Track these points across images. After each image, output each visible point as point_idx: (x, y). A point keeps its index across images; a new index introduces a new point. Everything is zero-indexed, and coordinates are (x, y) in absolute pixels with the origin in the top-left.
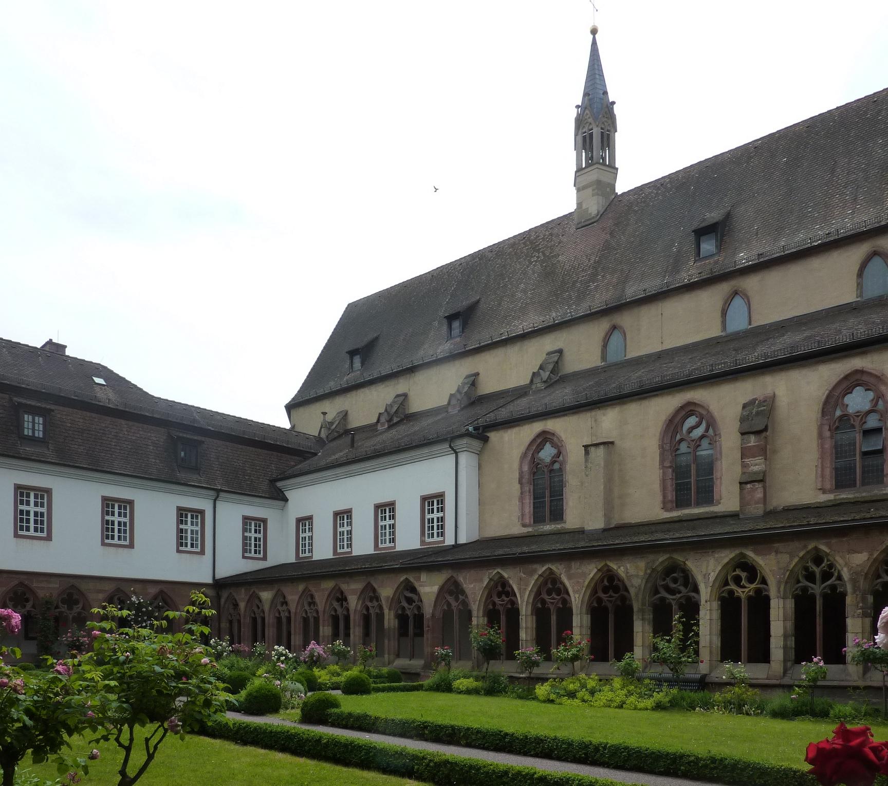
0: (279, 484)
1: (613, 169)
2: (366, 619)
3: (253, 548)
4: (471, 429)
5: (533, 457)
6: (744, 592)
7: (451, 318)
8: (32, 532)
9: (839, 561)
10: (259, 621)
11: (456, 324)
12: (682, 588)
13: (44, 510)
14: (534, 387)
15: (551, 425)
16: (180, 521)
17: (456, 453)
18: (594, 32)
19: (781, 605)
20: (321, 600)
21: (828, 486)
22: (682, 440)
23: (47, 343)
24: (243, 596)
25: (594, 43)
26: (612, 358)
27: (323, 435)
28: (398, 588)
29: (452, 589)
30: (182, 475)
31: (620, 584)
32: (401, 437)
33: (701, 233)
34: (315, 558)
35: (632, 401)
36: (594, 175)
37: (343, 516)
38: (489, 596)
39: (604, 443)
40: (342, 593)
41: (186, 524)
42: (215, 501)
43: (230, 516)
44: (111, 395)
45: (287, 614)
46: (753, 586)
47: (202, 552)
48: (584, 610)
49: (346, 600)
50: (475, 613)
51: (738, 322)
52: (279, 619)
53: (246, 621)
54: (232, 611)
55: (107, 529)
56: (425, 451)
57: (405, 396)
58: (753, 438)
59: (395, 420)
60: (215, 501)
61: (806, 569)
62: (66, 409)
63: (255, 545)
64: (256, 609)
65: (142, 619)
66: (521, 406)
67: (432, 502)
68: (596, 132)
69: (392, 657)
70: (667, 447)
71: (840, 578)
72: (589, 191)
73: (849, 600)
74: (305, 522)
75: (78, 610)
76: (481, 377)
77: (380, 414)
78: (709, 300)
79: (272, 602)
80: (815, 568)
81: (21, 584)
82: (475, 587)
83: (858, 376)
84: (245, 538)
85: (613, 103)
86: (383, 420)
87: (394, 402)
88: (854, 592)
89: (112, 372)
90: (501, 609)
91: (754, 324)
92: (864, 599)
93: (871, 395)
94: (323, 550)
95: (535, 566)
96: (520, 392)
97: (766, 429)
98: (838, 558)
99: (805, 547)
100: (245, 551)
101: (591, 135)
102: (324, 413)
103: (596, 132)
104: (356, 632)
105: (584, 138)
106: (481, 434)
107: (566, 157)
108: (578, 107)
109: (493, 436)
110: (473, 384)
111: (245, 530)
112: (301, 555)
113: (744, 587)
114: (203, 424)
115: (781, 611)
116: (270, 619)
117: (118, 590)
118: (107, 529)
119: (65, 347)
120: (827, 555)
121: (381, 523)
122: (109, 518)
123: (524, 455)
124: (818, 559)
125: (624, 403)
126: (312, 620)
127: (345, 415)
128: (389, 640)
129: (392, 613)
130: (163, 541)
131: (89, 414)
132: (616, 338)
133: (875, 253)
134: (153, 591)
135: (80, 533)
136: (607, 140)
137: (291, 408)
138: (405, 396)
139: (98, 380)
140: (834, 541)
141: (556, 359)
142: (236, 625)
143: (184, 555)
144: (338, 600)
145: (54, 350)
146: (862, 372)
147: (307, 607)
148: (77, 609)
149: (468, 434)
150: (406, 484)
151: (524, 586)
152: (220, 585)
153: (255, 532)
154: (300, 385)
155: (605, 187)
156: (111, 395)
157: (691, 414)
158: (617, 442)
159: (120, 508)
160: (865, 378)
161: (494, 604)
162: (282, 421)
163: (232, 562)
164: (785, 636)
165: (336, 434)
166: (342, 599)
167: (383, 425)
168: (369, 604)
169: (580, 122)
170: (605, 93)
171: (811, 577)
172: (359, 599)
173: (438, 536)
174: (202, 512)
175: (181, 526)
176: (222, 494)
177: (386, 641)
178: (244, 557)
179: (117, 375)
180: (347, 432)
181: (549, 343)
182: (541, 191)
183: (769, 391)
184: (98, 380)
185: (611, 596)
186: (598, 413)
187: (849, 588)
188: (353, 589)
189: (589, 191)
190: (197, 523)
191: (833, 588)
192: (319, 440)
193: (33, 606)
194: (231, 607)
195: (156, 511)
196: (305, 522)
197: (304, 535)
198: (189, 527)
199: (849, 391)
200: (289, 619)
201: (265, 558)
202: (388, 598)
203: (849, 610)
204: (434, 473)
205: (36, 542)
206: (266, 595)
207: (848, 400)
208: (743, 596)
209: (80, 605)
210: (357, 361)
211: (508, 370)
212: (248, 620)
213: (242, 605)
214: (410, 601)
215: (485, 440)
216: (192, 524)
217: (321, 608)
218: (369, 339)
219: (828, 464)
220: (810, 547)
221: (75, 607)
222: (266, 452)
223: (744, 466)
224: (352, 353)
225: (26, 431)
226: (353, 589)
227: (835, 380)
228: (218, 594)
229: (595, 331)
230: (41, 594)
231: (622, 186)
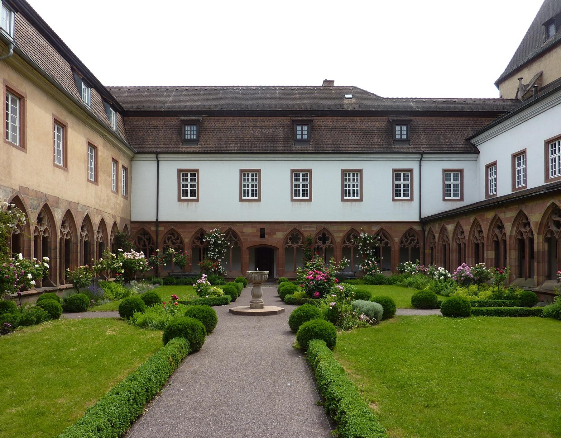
0: (473, 141)
2: (521, 242)
8: (301, 197)
13: (182, 183)
20: (467, 228)
23: (324, 81)
24: (437, 229)
27: (520, 97)
28: (545, 213)
37: (519, 156)
42: (420, 161)
43: (431, 175)
47: (412, 200)
55: (346, 191)
60: (420, 161)
65: (367, 248)
69: (541, 278)
74: (491, 166)
75: (329, 244)
81: (295, 229)
89: (359, 89)
94: (504, 189)
117: (353, 229)
118: (195, 191)
119: (333, 81)
122: (398, 183)
128: (538, 262)
129: (541, 237)
130: (376, 193)
131: (336, 118)
134: (375, 229)
137: (498, 84)
148: (328, 243)
152: (424, 222)
153: (452, 181)
154: (508, 64)
159: (354, 175)
162: (494, 93)
163: (434, 203)
168: (523, 230)
172: (513, 226)
173: (191, 196)
174: (411, 171)
176: (425, 156)
177: (535, 264)
190: (357, 179)
193: (303, 243)
195: (377, 174)
196: (491, 166)
201: (462, 199)
202: (537, 223)
205: (354, 203)
206: (450, 227)
209: (330, 241)
210: (552, 29)
212: (441, 247)
213: (437, 236)
222: (464, 118)
225: (298, 136)
228: (423, 228)
230: (306, 235)
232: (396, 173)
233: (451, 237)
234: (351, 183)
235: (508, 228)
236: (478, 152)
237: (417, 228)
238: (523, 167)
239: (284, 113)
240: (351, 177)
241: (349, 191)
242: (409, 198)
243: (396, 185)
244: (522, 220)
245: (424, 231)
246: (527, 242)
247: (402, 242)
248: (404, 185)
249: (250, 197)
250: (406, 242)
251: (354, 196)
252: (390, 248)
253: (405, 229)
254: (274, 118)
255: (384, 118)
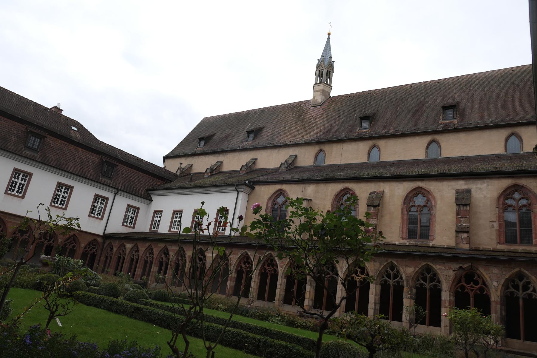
0: (150, 192)
1: (330, 86)
2: (177, 267)
3: (129, 221)
4: (247, 182)
5: (274, 201)
6: (358, 278)
7: (249, 132)
9: (401, 270)
10: (122, 259)
11: (251, 136)
12: (330, 272)
14: (281, 169)
15: (284, 187)
16: (95, 201)
17: (238, 192)
18: (329, 34)
19: (374, 288)
20: (156, 251)
21: (404, 236)
22: (342, 204)
25: (329, 38)
26: (318, 164)
27: (178, 173)
29: (246, 260)
30: (103, 179)
31: (275, 263)
32: (216, 180)
33: (363, 118)
34: (159, 232)
35: (322, 183)
36: (321, 87)
38: (240, 263)
39: (307, 199)
40: (167, 250)
41: (97, 203)
43: (120, 205)
44: (78, 136)
45: (137, 257)
46: (363, 276)
47: (102, 219)
48: (284, 276)
49: (169, 254)
50: (280, 276)
51: (374, 159)
52: (132, 260)
53: (115, 258)
54: (109, 252)
55: (11, 187)
56: (224, 188)
57: (222, 162)
58: (372, 208)
59: (214, 173)
61: (387, 271)
62: (53, 138)
63: (130, 220)
64: (122, 253)
66: (274, 177)
67: (223, 212)
68: (325, 71)
70: (335, 206)
71: (401, 278)
72: (319, 93)
73: (405, 289)
76: (258, 161)
77: (243, 166)
78: (363, 147)
79: (131, 250)
80: (427, 275)
82: (234, 258)
83: (420, 190)
84: (126, 215)
85: (333, 62)
86: (208, 171)
87: (215, 164)
88: (407, 286)
89: (82, 126)
90: (244, 270)
91: (381, 160)
92: (411, 290)
93: (425, 199)
94: (164, 228)
95: (264, 251)
96: (274, 171)
97: (378, 205)
98: (401, 269)
99: (387, 261)
100: (124, 222)
101: (323, 72)
102: (181, 164)
103: (325, 71)
104: (170, 272)
105: (320, 72)
106: (251, 186)
107: (311, 78)
108: (319, 60)
109: (257, 188)
110: (254, 163)
111: (127, 211)
112: (152, 229)
113: (359, 276)
114: (120, 157)
115: (374, 290)
116: (128, 259)
120: (396, 266)
121: (174, 219)
122: (15, 180)
123: (270, 199)
124: (392, 267)
125: (318, 183)
126: (149, 262)
127: (191, 166)
131: (64, 142)
132: (321, 154)
133: (513, 134)
135: (38, 198)
136: (329, 75)
137: (165, 158)
138: (222, 162)
139: (73, 128)
140: (399, 260)
141: (293, 159)
142: (109, 259)
143: (92, 218)
144: (165, 254)
145: (57, 110)
146: (421, 188)
147: (148, 255)
149: (246, 185)
150: (213, 202)
151: (408, 271)
152: (106, 237)
155: (326, 94)
156: (78, 136)
157: (347, 193)
158: (313, 200)
159: (65, 189)
160: (423, 191)
161: (241, 267)
162: (160, 163)
163: (115, 224)
164: (375, 303)
165: (184, 174)
166: (167, 254)
167: (208, 174)
169: (318, 66)
170: (331, 57)
171: (389, 276)
174: (107, 199)
175: (95, 204)
176: (120, 192)
178: (123, 225)
179: (84, 128)
180: (190, 174)
181: (292, 151)
182: (300, 89)
183: (381, 189)
184: (73, 128)
185: (472, 287)
186: (306, 186)
187: (405, 285)
188: (173, 250)
189: (319, 93)
191: (398, 282)
192: (175, 175)
194: (109, 249)
195: (83, 195)
197: (156, 219)
198: (98, 205)
199: (416, 195)
200: (137, 260)
201: (134, 227)
202: (190, 256)
203: (405, 294)
204: (227, 199)
206: (129, 246)
207: (415, 199)
208: (358, 280)
209: (28, 235)
210: (203, 143)
211: (270, 160)
212: (116, 257)
213: (115, 249)
214: (200, 259)
215: (253, 189)
216: (101, 203)
217: (155, 256)
218: (210, 136)
219: (405, 226)
220: (389, 261)
221: (25, 235)
223: (458, 221)
224: (201, 139)
226: (173, 250)
227: (409, 190)
229: (312, 151)
231: (333, 94)
232: (97, 197)
233: (127, 252)
234: (62, 194)
235: (172, 254)
236: (152, 201)
237: (99, 240)
238: (178, 219)
239: (22, 121)
240: (63, 190)
241: (58, 199)
242: (100, 217)
243: (57, 194)
244: (181, 254)
245: (104, 243)
246: (122, 259)
247: (85, 248)
248: (63, 196)
249: (15, 193)
250: (89, 248)
251: (60, 204)
252: (75, 250)
253: (91, 238)
254: (12, 121)
255: (99, 156)
